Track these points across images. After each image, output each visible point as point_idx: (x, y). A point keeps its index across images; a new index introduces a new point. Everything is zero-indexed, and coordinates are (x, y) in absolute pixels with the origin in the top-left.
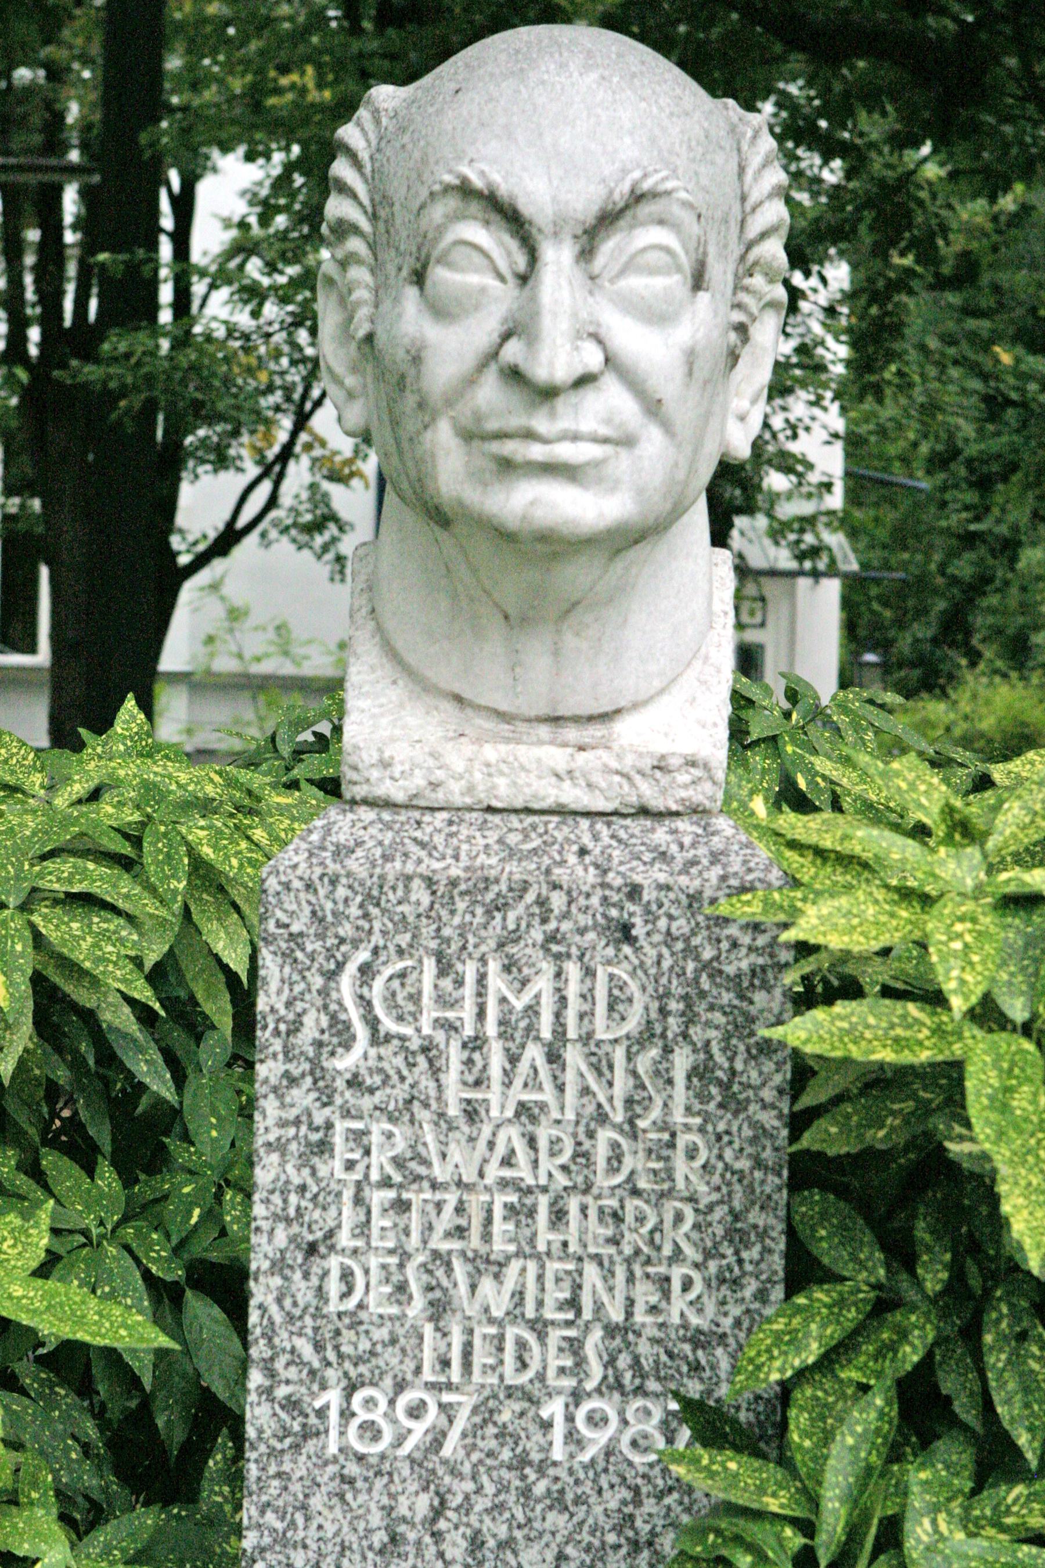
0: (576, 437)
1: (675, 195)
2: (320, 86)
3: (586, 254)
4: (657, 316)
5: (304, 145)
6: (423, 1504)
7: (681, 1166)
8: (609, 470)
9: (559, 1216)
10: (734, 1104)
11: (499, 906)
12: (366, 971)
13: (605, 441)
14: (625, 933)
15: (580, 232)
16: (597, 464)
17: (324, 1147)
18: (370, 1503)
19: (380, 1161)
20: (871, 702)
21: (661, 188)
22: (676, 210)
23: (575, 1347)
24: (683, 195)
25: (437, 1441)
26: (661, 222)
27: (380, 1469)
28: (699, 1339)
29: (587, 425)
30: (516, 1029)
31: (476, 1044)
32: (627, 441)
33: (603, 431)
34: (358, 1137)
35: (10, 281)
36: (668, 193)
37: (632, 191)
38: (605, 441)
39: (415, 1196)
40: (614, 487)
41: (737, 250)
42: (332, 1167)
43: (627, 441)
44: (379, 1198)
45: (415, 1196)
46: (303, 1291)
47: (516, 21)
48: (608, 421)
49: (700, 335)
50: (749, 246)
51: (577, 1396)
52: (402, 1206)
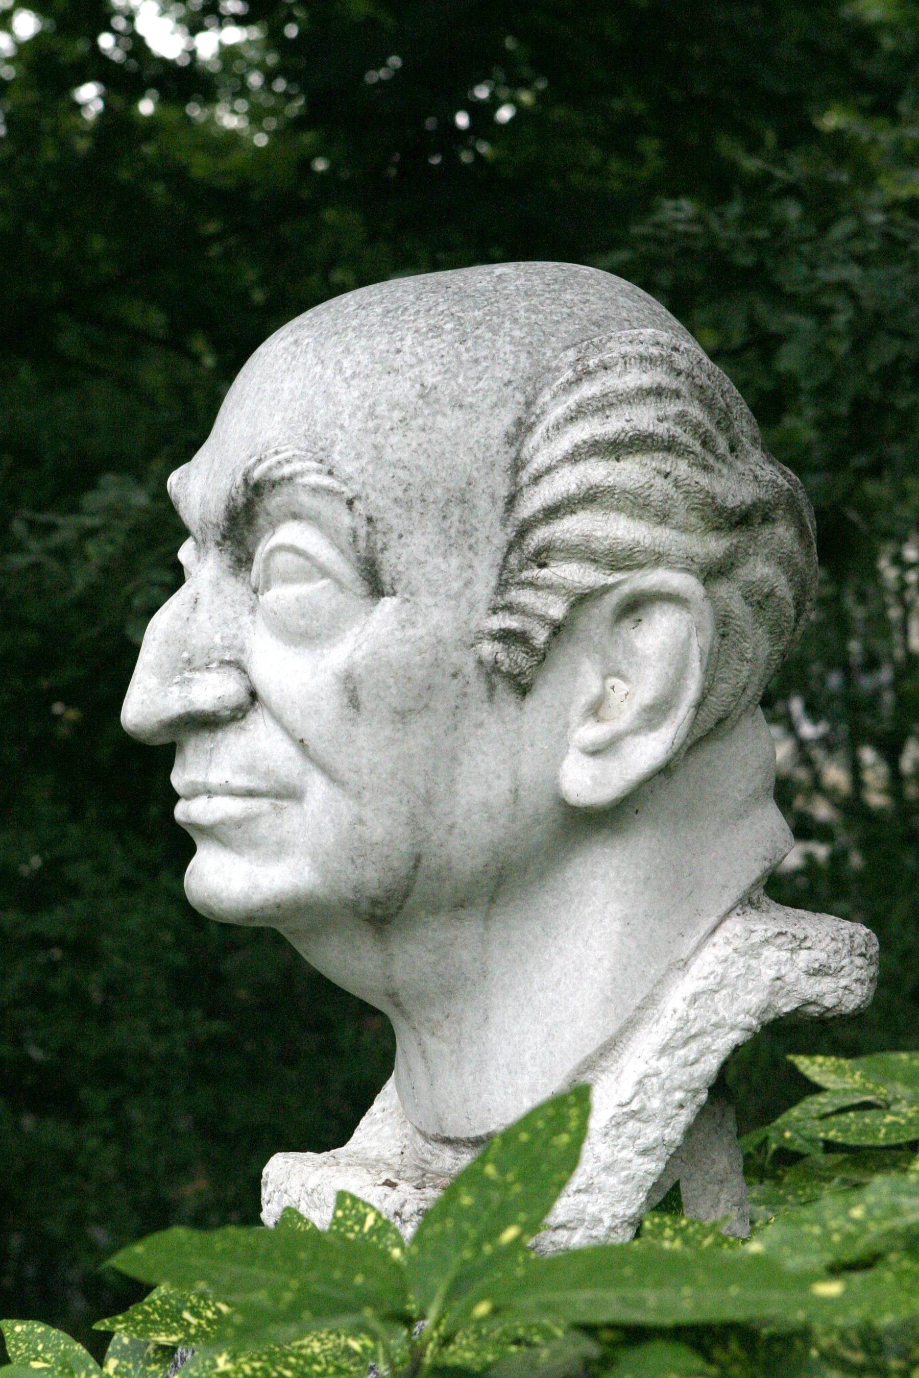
0: (210, 792)
1: (299, 480)
3: (242, 562)
4: (303, 634)
8: (263, 828)
13: (250, 794)
15: (219, 538)
16: (239, 823)
21: (277, 474)
22: (306, 500)
24: (313, 479)
26: (295, 516)
29: (215, 778)
32: (287, 794)
33: (241, 781)
36: (290, 479)
37: (246, 481)
38: (250, 794)
40: (280, 850)
41: (502, 537)
43: (287, 794)
47: (497, 252)
48: (251, 769)
49: (358, 656)
50: (524, 529)
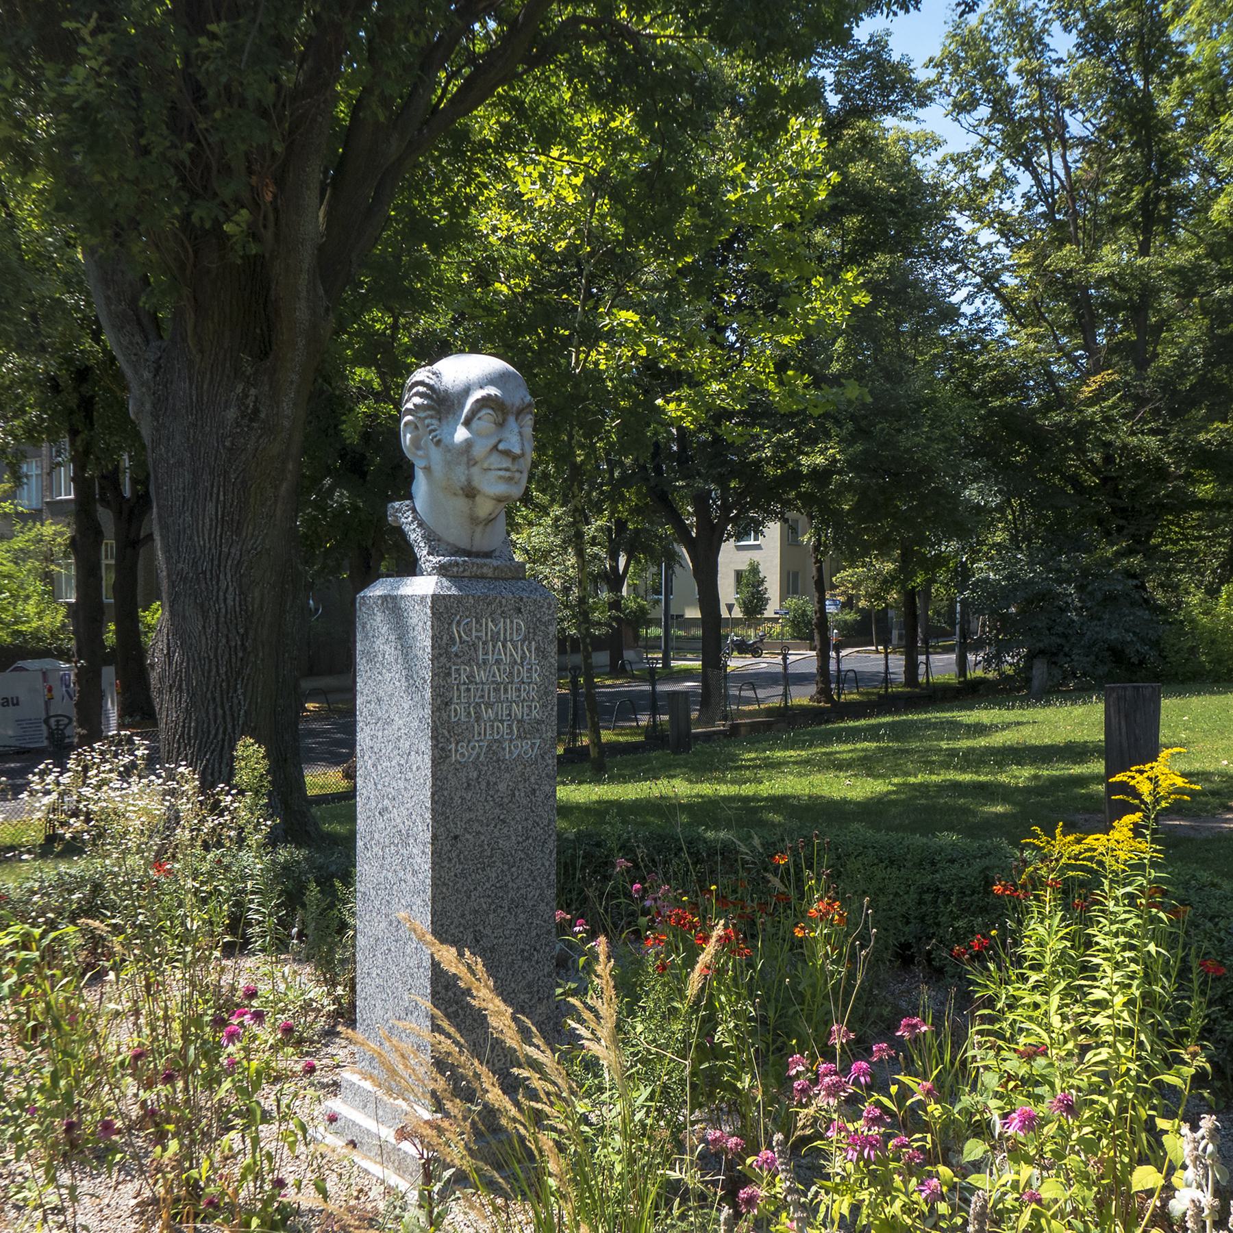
2: (1031, 563)
5: (551, 995)
6: (475, 774)
7: (535, 675)
9: (506, 690)
10: (545, 657)
11: (489, 604)
12: (459, 623)
14: (519, 611)
17: (449, 674)
18: (462, 775)
19: (464, 677)
20: (265, 227)
23: (510, 727)
25: (478, 755)
27: (464, 765)
28: (539, 722)
30: (495, 638)
31: (485, 643)
34: (457, 670)
35: (135, 620)
39: (472, 687)
42: (452, 680)
44: (463, 688)
45: (472, 687)
46: (445, 717)
51: (511, 740)
52: (468, 690)
